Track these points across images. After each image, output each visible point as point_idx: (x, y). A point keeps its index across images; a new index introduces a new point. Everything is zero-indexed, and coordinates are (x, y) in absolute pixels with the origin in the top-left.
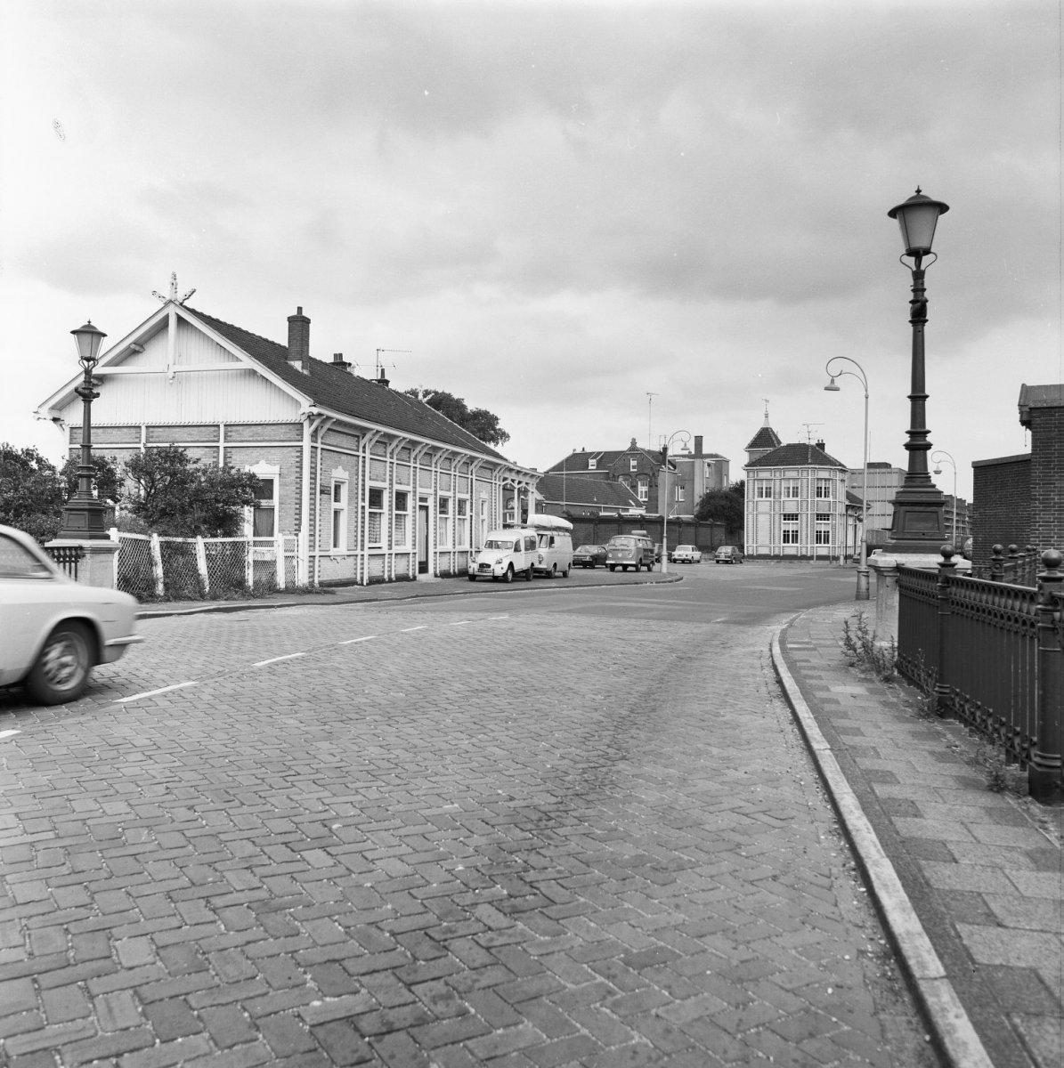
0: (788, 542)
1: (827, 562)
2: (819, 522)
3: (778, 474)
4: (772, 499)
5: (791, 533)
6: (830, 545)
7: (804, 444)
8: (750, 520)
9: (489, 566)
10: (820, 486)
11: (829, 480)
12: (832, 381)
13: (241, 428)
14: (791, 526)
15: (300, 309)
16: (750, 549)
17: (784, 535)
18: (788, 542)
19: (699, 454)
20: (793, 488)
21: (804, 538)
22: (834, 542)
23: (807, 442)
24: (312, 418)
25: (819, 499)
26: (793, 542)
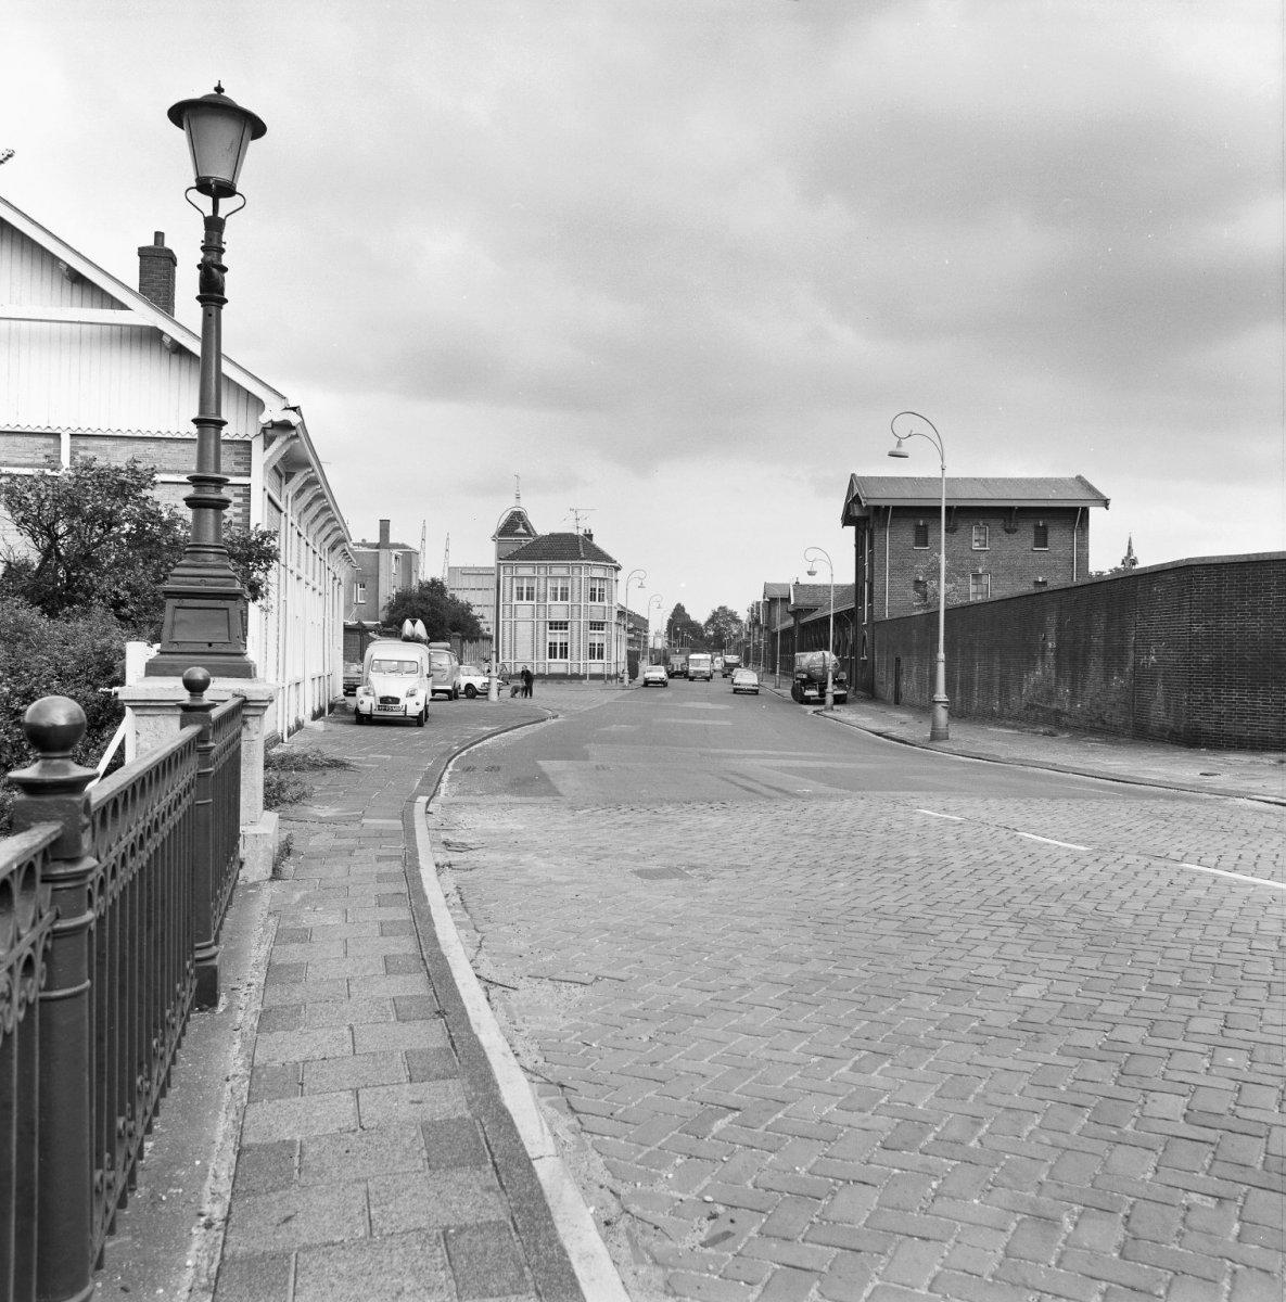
0: (555, 657)
1: (602, 682)
2: (593, 632)
3: (542, 571)
4: (534, 602)
5: (558, 646)
6: (605, 661)
7: (572, 535)
8: (507, 629)
9: (396, 701)
10: (593, 586)
11: (604, 579)
12: (899, 444)
13: (110, 443)
14: (558, 637)
15: (159, 236)
16: (541, 666)
17: (550, 648)
18: (555, 657)
19: (384, 542)
20: (562, 589)
21: (575, 652)
22: (609, 658)
23: (575, 532)
24: (269, 432)
25: (593, 603)
26: (561, 657)
